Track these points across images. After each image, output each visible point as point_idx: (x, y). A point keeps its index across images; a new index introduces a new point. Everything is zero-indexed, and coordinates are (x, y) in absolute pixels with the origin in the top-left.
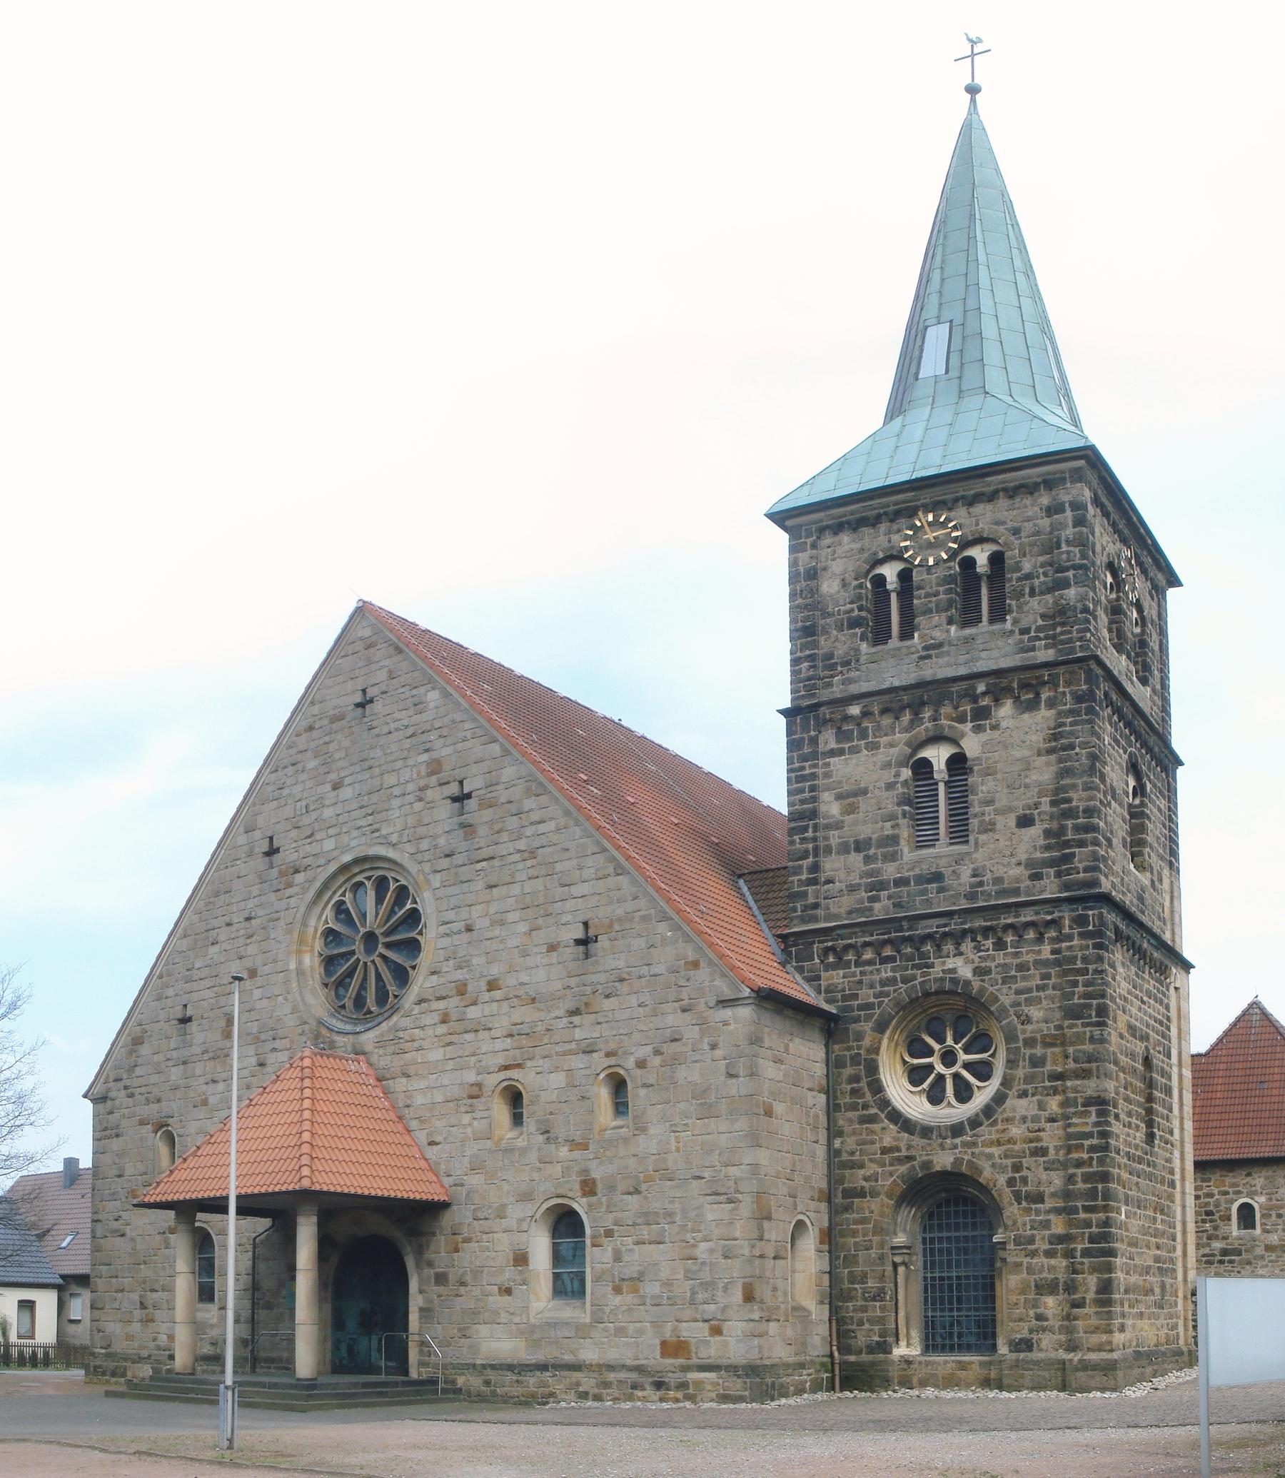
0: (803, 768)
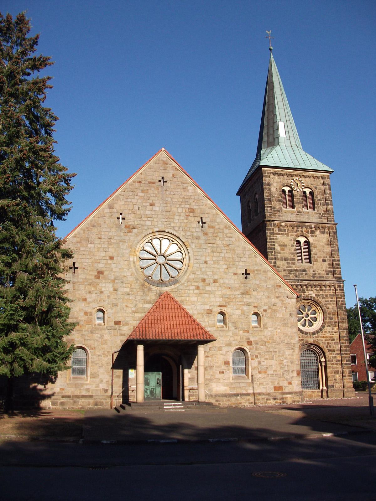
0: (271, 236)
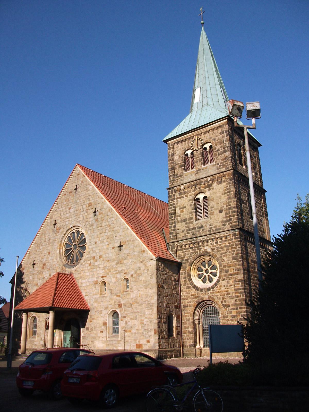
0: (172, 202)
